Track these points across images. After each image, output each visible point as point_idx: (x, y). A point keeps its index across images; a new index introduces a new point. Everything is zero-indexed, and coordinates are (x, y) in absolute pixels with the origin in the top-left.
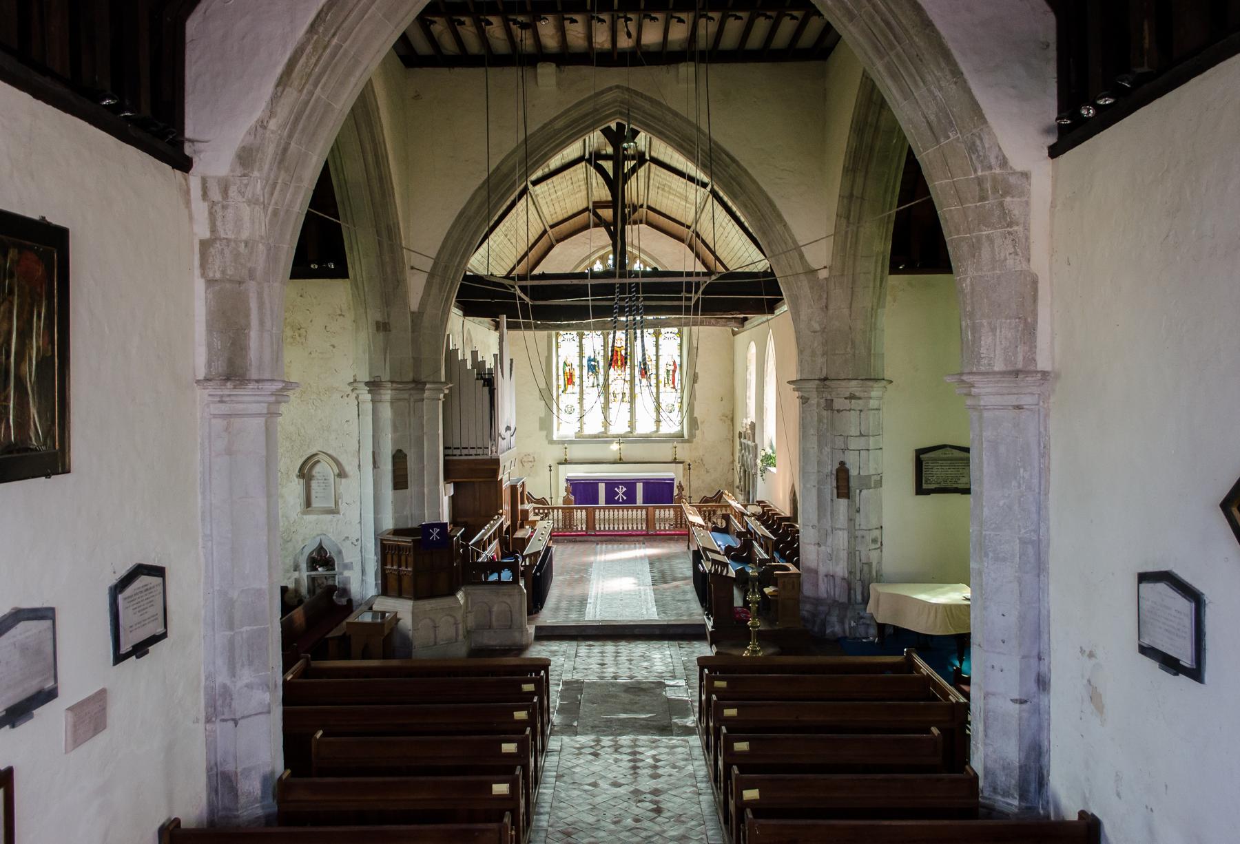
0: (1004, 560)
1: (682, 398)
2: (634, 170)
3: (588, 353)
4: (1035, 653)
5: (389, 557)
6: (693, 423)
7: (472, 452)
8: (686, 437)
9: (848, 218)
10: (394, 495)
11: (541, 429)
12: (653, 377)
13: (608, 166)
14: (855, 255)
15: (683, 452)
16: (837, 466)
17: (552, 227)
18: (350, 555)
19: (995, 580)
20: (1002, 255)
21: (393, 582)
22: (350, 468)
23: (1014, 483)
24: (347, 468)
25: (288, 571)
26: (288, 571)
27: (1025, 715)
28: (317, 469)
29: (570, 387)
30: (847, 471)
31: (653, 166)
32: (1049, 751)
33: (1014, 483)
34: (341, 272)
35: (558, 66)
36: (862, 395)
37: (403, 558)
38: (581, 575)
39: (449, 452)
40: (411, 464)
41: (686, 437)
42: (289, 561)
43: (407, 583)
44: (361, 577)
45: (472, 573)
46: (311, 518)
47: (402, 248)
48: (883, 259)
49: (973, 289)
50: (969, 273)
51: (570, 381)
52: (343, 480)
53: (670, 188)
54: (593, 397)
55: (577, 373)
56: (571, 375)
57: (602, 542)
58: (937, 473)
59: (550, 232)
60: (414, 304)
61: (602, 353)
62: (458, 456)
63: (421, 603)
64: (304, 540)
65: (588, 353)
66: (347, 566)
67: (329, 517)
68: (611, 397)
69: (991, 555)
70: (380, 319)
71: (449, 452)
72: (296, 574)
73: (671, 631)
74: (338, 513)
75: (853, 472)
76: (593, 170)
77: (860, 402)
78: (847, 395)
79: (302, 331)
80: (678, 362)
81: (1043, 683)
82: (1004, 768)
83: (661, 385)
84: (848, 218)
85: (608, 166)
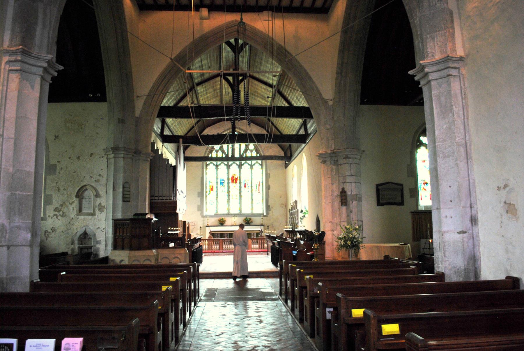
0: (448, 156)
2: (242, 80)
4: (468, 205)
5: (118, 230)
6: (268, 207)
7: (164, 198)
8: (265, 214)
9: (341, 73)
10: (123, 204)
11: (198, 210)
13: (231, 79)
16: (341, 190)
18: (101, 236)
19: (444, 169)
20: (434, 3)
21: (119, 241)
22: (102, 192)
23: (451, 115)
24: (101, 193)
25: (68, 244)
27: (465, 240)
28: (86, 193)
30: (345, 192)
31: (251, 80)
32: (480, 258)
33: (451, 115)
34: (103, 99)
35: (209, 11)
36: (351, 156)
37: (125, 230)
39: (153, 198)
40: (133, 190)
41: (265, 214)
43: (126, 241)
44: (104, 245)
45: (160, 241)
46: (81, 217)
47: (127, 32)
49: (420, 22)
50: (418, 15)
51: (212, 189)
52: (98, 199)
53: (258, 93)
54: (223, 196)
60: (137, 113)
62: (158, 200)
63: (133, 252)
64: (77, 229)
67: (90, 217)
69: (441, 155)
71: (153, 198)
72: (73, 246)
74: (95, 215)
75: (349, 193)
76: (224, 81)
78: (344, 156)
79: (83, 126)
80: (261, 182)
81: (474, 220)
82: (455, 272)
84: (341, 73)
85: (231, 79)
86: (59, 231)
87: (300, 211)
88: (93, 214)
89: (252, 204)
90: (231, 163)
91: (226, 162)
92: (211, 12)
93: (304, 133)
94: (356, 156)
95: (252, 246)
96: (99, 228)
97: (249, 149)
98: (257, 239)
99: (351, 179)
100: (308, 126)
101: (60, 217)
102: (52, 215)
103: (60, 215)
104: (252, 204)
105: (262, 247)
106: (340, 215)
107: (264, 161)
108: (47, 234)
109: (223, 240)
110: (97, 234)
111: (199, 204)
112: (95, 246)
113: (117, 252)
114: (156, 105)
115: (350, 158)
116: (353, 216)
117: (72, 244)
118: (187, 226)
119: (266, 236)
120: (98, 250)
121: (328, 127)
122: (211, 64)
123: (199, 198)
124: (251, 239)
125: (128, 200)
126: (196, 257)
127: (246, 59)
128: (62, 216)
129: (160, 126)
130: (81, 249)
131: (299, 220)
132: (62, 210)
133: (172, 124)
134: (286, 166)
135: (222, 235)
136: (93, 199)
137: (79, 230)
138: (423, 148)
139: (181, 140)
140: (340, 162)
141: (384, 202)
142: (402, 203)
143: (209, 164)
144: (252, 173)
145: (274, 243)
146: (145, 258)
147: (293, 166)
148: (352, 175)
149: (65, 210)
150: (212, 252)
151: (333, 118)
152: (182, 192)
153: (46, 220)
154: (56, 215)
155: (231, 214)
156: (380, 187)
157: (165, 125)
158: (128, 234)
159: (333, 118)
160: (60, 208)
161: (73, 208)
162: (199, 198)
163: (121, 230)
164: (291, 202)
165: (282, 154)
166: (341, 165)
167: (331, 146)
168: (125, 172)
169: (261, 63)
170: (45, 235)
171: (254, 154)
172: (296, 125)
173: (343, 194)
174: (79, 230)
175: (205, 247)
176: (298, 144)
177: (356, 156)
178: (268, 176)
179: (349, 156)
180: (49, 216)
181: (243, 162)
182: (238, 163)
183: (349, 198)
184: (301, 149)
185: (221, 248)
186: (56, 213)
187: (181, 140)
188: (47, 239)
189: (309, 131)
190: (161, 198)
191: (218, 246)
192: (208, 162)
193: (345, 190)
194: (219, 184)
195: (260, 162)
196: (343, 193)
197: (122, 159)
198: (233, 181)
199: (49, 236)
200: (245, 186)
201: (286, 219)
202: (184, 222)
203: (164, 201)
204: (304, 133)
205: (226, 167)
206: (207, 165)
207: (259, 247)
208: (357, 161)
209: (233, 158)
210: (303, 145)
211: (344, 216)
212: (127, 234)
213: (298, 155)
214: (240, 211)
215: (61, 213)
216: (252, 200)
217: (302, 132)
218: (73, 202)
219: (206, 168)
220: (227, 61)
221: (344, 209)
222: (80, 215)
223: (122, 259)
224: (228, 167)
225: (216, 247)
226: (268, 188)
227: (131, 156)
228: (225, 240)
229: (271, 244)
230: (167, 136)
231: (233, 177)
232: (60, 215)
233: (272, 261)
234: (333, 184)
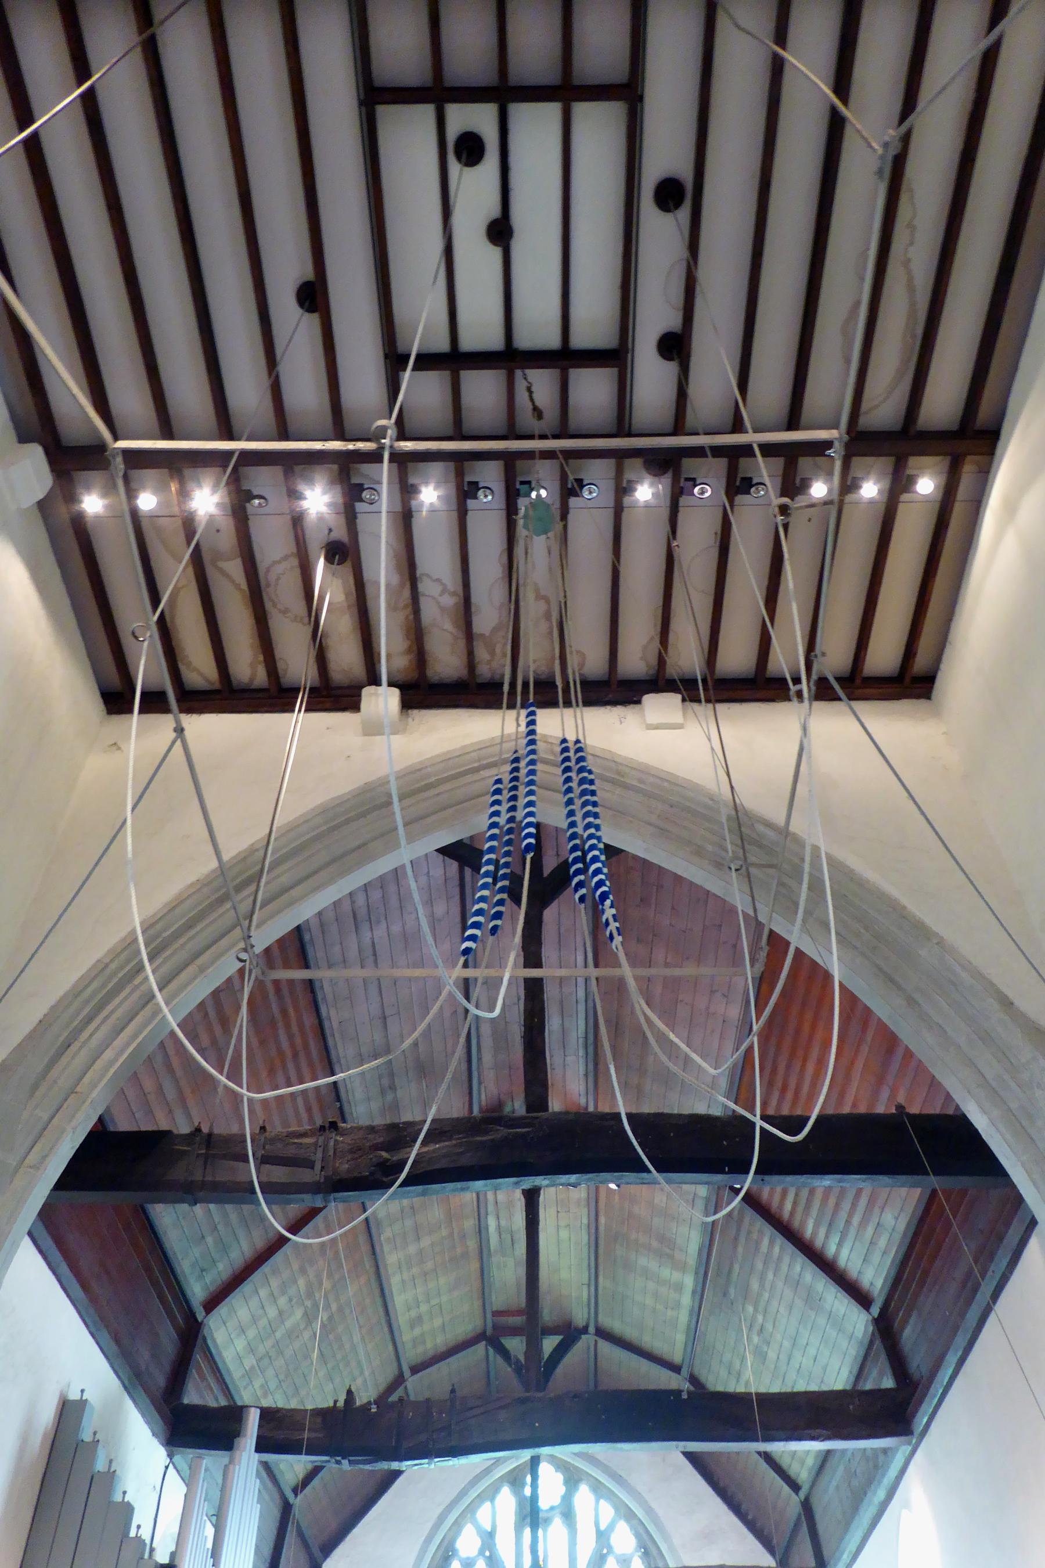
17: (415, 1370)
93: (888, 1383)
133: (249, 1375)
157: (198, 1357)
204: (888, 1383)
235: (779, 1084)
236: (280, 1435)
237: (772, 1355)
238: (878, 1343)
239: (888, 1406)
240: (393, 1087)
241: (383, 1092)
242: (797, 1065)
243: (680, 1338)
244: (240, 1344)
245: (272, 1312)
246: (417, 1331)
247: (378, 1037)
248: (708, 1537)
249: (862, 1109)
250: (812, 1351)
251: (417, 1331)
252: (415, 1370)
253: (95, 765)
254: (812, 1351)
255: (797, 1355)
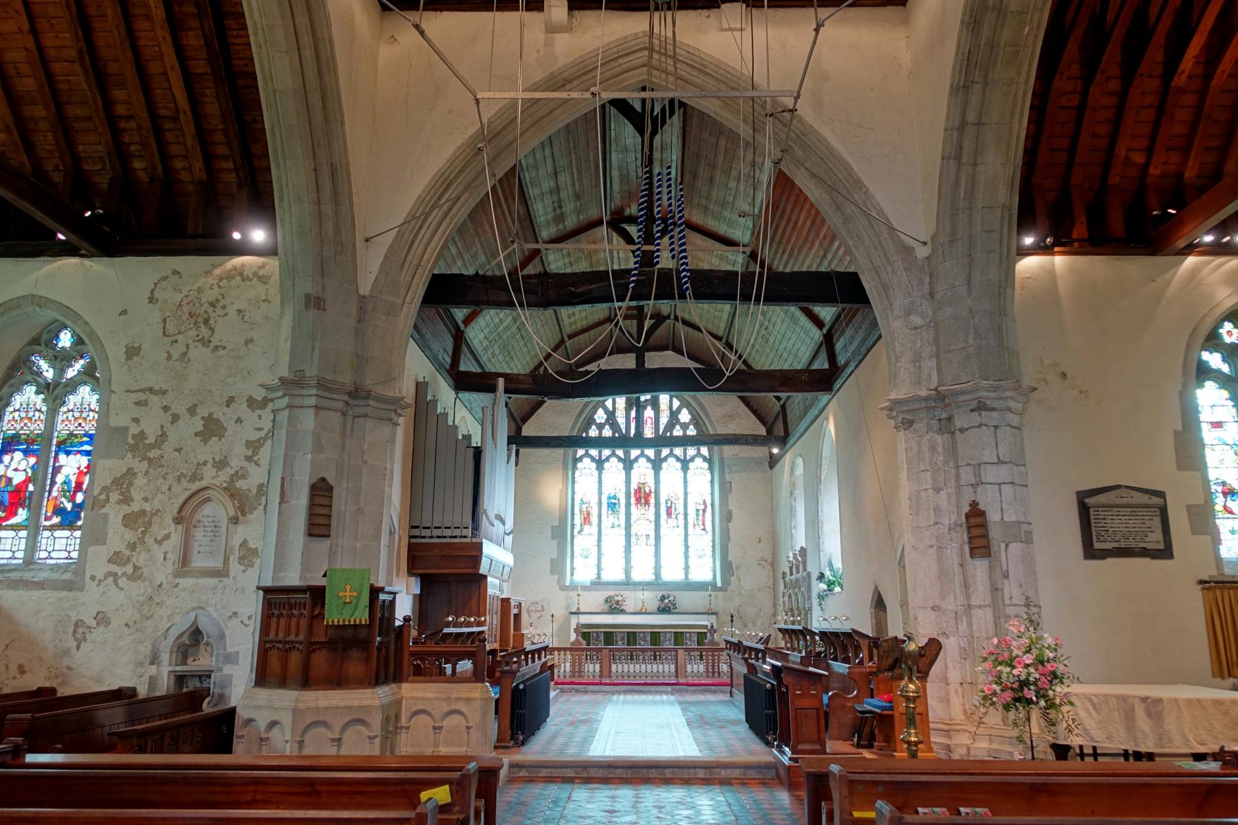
1: (713, 541)
3: (608, 490)
6: (727, 568)
7: (447, 532)
8: (719, 584)
9: (958, 158)
10: (305, 544)
11: (552, 572)
12: (681, 517)
14: (970, 208)
15: (719, 602)
16: (967, 509)
17: (571, 337)
25: (141, 664)
26: (141, 664)
28: (208, 509)
29: (586, 527)
30: (982, 514)
36: (995, 404)
38: (590, 724)
39: (416, 532)
41: (719, 584)
42: (145, 649)
46: (185, 582)
48: (1010, 216)
51: (587, 520)
54: (614, 540)
55: (595, 512)
56: (588, 514)
57: (619, 693)
58: (1115, 527)
59: (568, 343)
61: (624, 489)
62: (429, 537)
65: (608, 490)
66: (231, 659)
68: (633, 539)
70: (311, 291)
71: (416, 532)
72: (154, 668)
73: (724, 773)
74: (227, 576)
75: (993, 516)
77: (994, 414)
78: (974, 404)
80: (709, 502)
83: (690, 526)
86: (115, 622)
87: (815, 575)
88: (221, 573)
89: (687, 557)
90: (635, 453)
91: (620, 452)
92: (576, 13)
93: (826, 366)
94: (1011, 404)
95: (689, 667)
96: (235, 614)
97: (678, 420)
98: (701, 651)
99: (1001, 473)
100: (839, 346)
101: (123, 582)
102: (100, 576)
103: (124, 574)
104: (687, 557)
105: (713, 671)
106: (966, 586)
107: (716, 448)
108: (80, 630)
109: (610, 650)
110: (227, 633)
111: (555, 557)
112: (220, 670)
113: (264, 694)
114: (419, 265)
115: (993, 409)
116: (1012, 591)
117: (152, 663)
118: (514, 611)
119: (727, 642)
120: (227, 682)
121: (918, 320)
122: (581, 184)
123: (555, 542)
124: (686, 650)
125: (324, 531)
126: (522, 713)
127: (674, 156)
128: (132, 578)
129: (450, 346)
130: (181, 679)
131: (815, 601)
132: (134, 559)
133: (486, 349)
134: (773, 461)
135: (609, 636)
136: (224, 529)
137: (177, 619)
138: (1210, 385)
139: (501, 381)
140: (959, 423)
141: (1109, 546)
142: (1166, 552)
143: (581, 459)
144: (685, 481)
145: (752, 668)
146: (350, 717)
147: (793, 463)
148: (1000, 462)
149: (141, 558)
150: (576, 683)
151: (932, 295)
152: (499, 518)
153: (82, 589)
154: (115, 575)
155: (639, 584)
156: (1088, 501)
157: (464, 348)
158: (301, 638)
159: (932, 295)
160: (127, 552)
161: (165, 553)
162: (555, 542)
163: (282, 621)
164: (788, 555)
165: (762, 431)
166: (962, 430)
167: (930, 375)
168: (318, 447)
169: (711, 180)
170: (75, 632)
171: (691, 431)
172: (803, 349)
173: (973, 521)
174: (177, 619)
175: (564, 666)
176: (810, 395)
177: (1011, 404)
178: (726, 488)
179: (988, 402)
180: (93, 578)
181: (665, 452)
182: (650, 452)
183: (995, 533)
184: (816, 412)
185: (606, 672)
186: (114, 568)
187: (501, 381)
188: (78, 647)
189: (841, 360)
190: (437, 532)
191: (598, 666)
192: (581, 452)
193: (981, 507)
194: (605, 507)
195: (704, 451)
196: (976, 518)
197: (311, 412)
198: (638, 500)
199: (85, 639)
200: (669, 514)
201: (775, 597)
202: (505, 602)
203: (448, 540)
204: (826, 366)
205: (621, 465)
206: (576, 460)
207: (707, 672)
208: (1014, 419)
209: (639, 441)
210: (824, 398)
211: (981, 592)
212: (297, 636)
213: (799, 438)
214: (657, 573)
215: (129, 569)
216: (687, 547)
217: (822, 363)
218: (167, 537)
219: (575, 468)
220: (625, 178)
221: (979, 568)
222: (184, 575)
223: (276, 718)
224: (628, 464)
225: (592, 668)
226: (727, 517)
227: (340, 405)
228: (618, 650)
229: (744, 670)
230: (468, 374)
231: (638, 491)
232: (124, 574)
233: (749, 719)
234: (937, 490)
235: (786, 217)
236: (512, 386)
237: (771, 340)
238: (824, 346)
239: (822, 380)
240: (560, 207)
241: (555, 210)
242: (797, 211)
243: (723, 326)
244: (481, 336)
245: (496, 320)
246: (572, 319)
247: (552, 183)
248: (730, 417)
249: (813, 269)
250: (792, 342)
251: (572, 319)
252: (571, 337)
253: (385, 53)
254: (792, 342)
255: (784, 343)
